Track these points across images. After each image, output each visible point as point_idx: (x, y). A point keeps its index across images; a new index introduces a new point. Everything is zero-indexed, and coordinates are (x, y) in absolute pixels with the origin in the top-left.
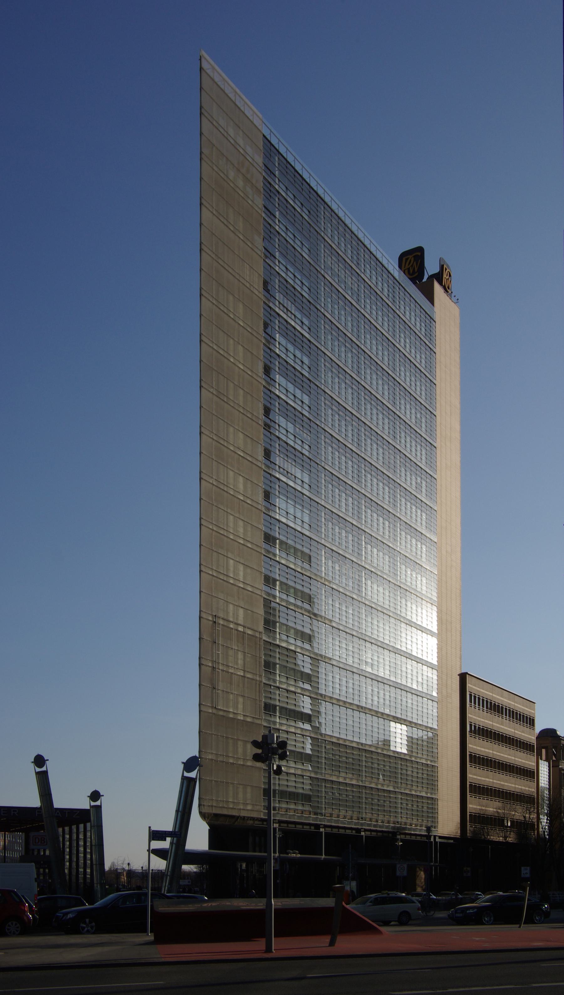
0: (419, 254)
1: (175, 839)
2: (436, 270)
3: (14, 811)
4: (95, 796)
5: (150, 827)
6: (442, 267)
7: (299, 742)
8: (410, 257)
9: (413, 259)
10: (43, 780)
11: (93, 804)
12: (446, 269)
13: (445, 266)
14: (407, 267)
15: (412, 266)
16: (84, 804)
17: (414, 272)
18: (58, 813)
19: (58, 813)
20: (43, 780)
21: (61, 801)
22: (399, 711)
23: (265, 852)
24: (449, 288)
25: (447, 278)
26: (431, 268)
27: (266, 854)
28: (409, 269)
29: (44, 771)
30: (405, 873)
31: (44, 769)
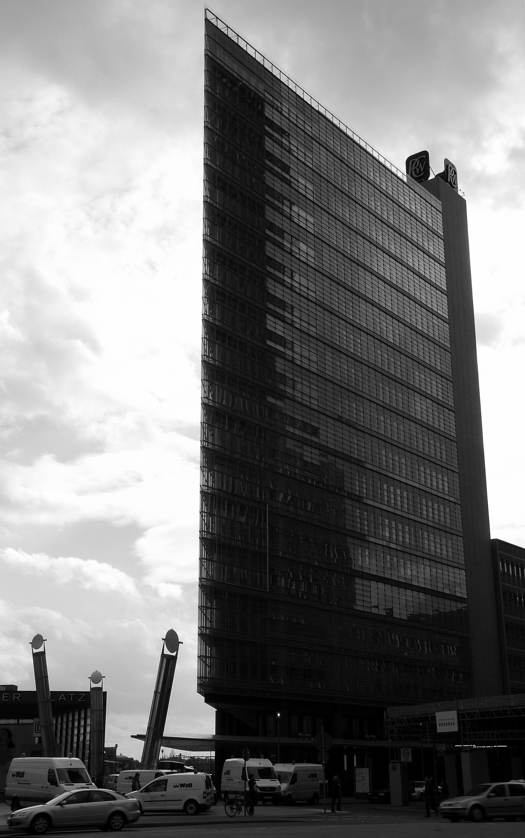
0: (424, 157)
1: (214, 758)
2: (442, 169)
3: (16, 696)
4: (96, 677)
5: (182, 643)
6: (447, 167)
7: (366, 586)
8: (416, 159)
9: (418, 162)
10: (39, 660)
11: (94, 685)
12: (451, 168)
13: (449, 166)
14: (413, 168)
15: (418, 167)
16: (84, 685)
17: (420, 172)
18: (62, 697)
19: (62, 697)
20: (39, 660)
21: (57, 683)
22: (421, 580)
23: (357, 764)
24: (454, 184)
25: (453, 175)
26: (436, 168)
27: (355, 766)
28: (415, 170)
29: (41, 652)
30: (410, 759)
31: (41, 649)
